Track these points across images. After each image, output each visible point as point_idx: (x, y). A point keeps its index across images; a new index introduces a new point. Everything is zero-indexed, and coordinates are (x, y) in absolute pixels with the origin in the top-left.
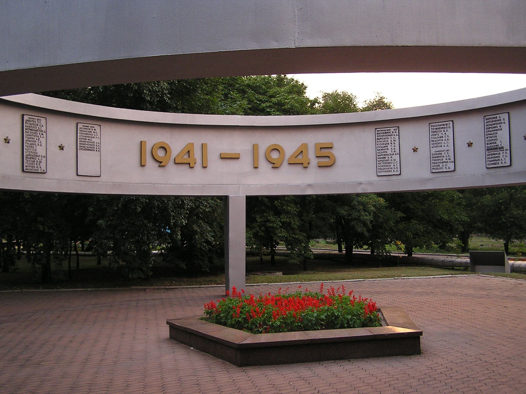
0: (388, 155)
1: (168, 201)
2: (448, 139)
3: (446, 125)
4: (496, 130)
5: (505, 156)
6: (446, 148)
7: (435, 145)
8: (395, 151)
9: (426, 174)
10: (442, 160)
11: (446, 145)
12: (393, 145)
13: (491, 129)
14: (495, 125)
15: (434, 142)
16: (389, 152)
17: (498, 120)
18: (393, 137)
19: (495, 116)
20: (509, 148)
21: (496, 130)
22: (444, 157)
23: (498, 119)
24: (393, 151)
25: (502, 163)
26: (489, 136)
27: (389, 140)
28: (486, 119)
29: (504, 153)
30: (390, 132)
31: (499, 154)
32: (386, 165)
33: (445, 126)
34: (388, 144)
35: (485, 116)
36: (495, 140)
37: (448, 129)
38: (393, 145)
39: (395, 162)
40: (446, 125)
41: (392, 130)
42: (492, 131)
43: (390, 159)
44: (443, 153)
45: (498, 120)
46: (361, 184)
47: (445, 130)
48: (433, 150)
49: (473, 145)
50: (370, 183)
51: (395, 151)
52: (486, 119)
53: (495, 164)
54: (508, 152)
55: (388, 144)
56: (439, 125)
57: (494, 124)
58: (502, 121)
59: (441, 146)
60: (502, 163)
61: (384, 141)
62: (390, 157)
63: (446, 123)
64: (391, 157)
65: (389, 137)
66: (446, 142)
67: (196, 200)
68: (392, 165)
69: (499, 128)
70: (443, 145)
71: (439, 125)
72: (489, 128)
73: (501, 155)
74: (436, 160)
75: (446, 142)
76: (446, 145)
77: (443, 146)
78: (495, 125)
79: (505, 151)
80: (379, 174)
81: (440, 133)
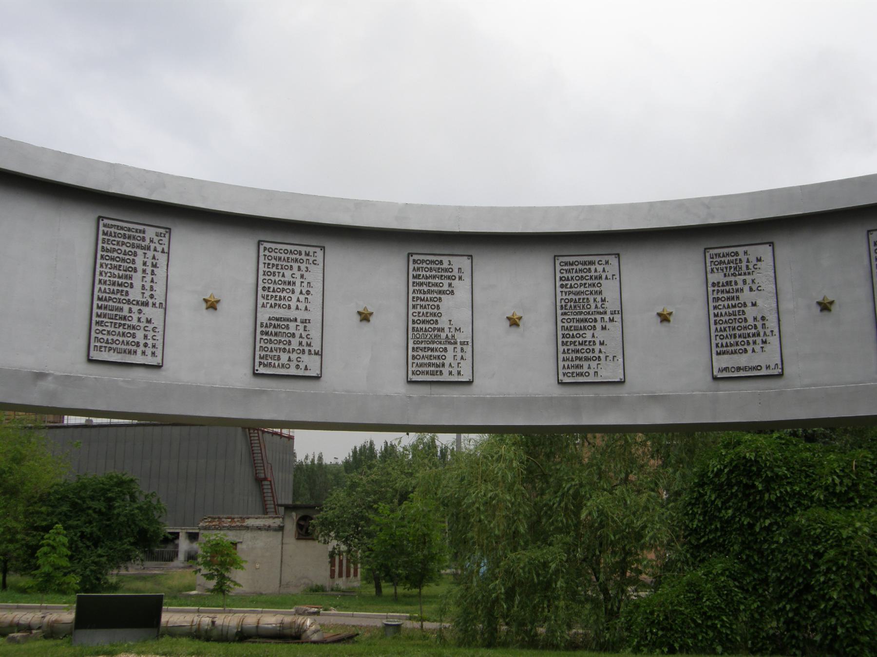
0: (129, 302)
1: (772, 471)
2: (308, 292)
3: (307, 254)
4: (440, 292)
5: (459, 357)
6: (300, 315)
7: (273, 302)
8: (152, 296)
9: (236, 373)
10: (290, 343)
11: (302, 306)
12: (149, 278)
13: (425, 288)
14: (437, 281)
15: (268, 290)
16: (135, 294)
17: (446, 270)
18: (150, 254)
19: (439, 258)
20: (470, 340)
21: (440, 292)
22: (293, 335)
23: (445, 265)
24: (148, 294)
25: (450, 373)
26: (419, 302)
27: (139, 260)
28: (415, 262)
29: (459, 349)
30: (144, 239)
31: (445, 350)
32: (121, 330)
33: (303, 257)
34: (135, 270)
35: (411, 254)
36: (435, 315)
37: (311, 267)
38: (149, 278)
39: (151, 326)
40: (307, 254)
41: (151, 232)
42: (429, 292)
43: (135, 316)
44: (292, 325)
45: (446, 270)
46: (41, 376)
47: (303, 266)
48: (264, 315)
49: (833, 308)
50: (67, 380)
51: (152, 296)
52: (415, 262)
53: (432, 373)
54: (468, 349)
55: (135, 270)
56: (286, 251)
57: (434, 277)
58: (455, 273)
59: (289, 307)
60: (450, 373)
61: (123, 260)
62: (135, 308)
63: (308, 249)
64: (140, 312)
65: (140, 252)
66: (302, 298)
67: (77, 508)
68: (140, 335)
69: (446, 288)
70: (293, 304)
71: (286, 251)
72: (421, 284)
73: (450, 354)
74: (271, 341)
75: (302, 298)
76: (302, 306)
77: (293, 307)
78: (437, 281)
79: (459, 346)
80: (95, 355)
81: (288, 273)
